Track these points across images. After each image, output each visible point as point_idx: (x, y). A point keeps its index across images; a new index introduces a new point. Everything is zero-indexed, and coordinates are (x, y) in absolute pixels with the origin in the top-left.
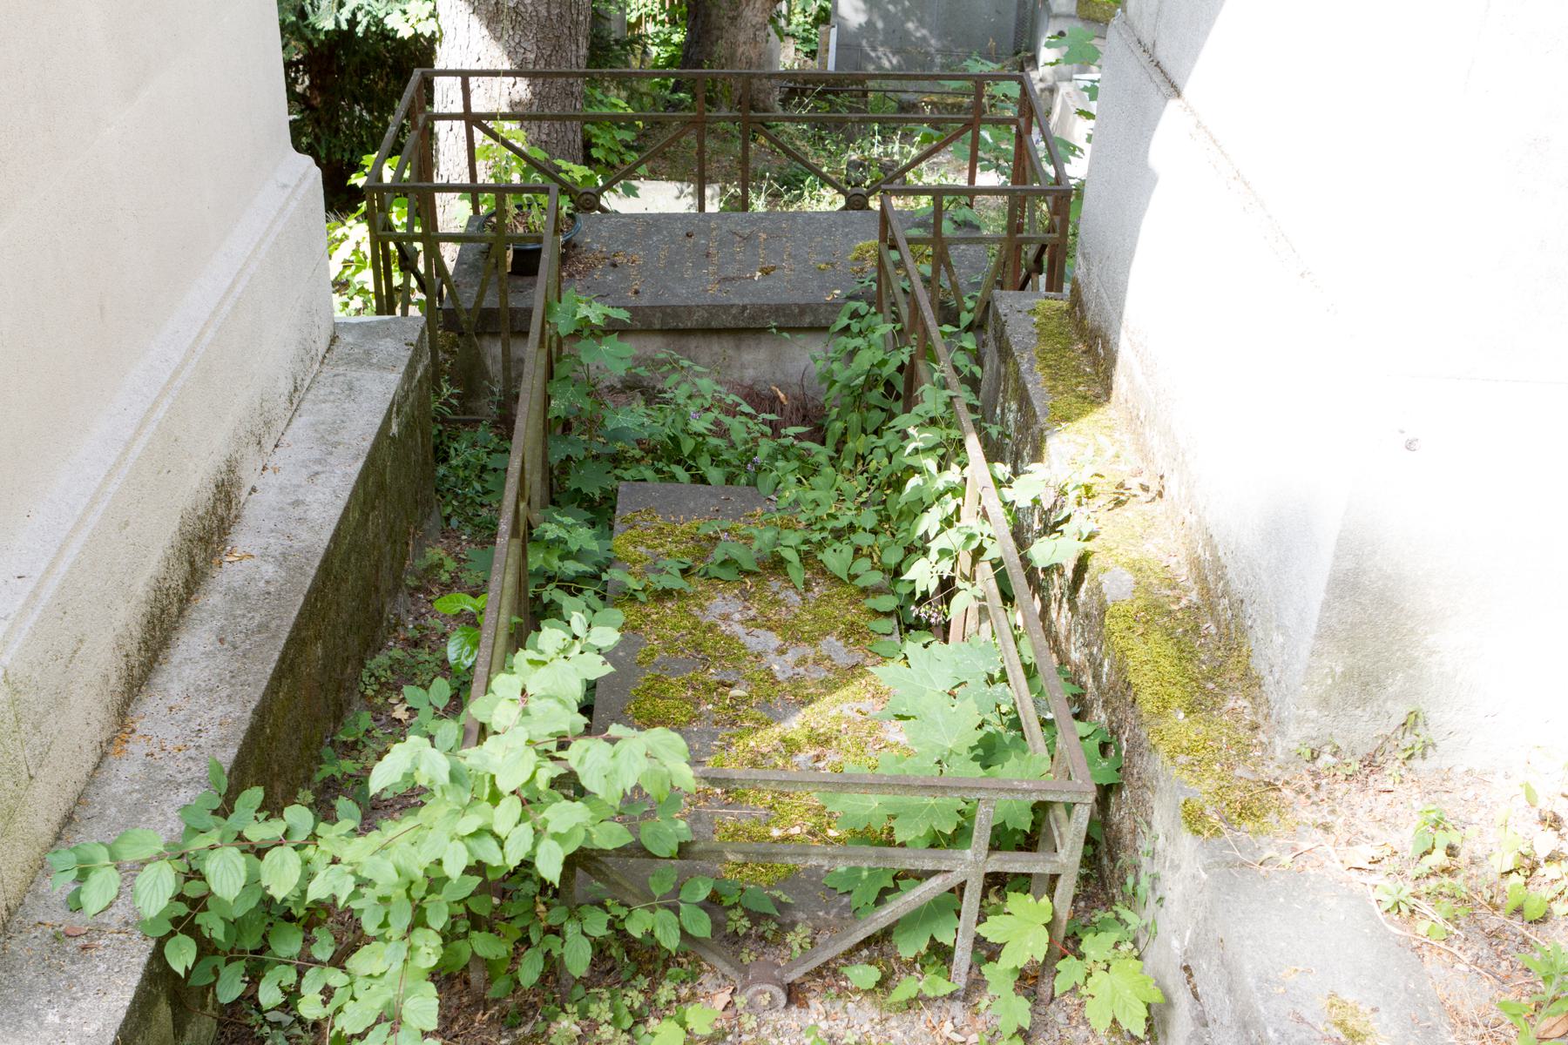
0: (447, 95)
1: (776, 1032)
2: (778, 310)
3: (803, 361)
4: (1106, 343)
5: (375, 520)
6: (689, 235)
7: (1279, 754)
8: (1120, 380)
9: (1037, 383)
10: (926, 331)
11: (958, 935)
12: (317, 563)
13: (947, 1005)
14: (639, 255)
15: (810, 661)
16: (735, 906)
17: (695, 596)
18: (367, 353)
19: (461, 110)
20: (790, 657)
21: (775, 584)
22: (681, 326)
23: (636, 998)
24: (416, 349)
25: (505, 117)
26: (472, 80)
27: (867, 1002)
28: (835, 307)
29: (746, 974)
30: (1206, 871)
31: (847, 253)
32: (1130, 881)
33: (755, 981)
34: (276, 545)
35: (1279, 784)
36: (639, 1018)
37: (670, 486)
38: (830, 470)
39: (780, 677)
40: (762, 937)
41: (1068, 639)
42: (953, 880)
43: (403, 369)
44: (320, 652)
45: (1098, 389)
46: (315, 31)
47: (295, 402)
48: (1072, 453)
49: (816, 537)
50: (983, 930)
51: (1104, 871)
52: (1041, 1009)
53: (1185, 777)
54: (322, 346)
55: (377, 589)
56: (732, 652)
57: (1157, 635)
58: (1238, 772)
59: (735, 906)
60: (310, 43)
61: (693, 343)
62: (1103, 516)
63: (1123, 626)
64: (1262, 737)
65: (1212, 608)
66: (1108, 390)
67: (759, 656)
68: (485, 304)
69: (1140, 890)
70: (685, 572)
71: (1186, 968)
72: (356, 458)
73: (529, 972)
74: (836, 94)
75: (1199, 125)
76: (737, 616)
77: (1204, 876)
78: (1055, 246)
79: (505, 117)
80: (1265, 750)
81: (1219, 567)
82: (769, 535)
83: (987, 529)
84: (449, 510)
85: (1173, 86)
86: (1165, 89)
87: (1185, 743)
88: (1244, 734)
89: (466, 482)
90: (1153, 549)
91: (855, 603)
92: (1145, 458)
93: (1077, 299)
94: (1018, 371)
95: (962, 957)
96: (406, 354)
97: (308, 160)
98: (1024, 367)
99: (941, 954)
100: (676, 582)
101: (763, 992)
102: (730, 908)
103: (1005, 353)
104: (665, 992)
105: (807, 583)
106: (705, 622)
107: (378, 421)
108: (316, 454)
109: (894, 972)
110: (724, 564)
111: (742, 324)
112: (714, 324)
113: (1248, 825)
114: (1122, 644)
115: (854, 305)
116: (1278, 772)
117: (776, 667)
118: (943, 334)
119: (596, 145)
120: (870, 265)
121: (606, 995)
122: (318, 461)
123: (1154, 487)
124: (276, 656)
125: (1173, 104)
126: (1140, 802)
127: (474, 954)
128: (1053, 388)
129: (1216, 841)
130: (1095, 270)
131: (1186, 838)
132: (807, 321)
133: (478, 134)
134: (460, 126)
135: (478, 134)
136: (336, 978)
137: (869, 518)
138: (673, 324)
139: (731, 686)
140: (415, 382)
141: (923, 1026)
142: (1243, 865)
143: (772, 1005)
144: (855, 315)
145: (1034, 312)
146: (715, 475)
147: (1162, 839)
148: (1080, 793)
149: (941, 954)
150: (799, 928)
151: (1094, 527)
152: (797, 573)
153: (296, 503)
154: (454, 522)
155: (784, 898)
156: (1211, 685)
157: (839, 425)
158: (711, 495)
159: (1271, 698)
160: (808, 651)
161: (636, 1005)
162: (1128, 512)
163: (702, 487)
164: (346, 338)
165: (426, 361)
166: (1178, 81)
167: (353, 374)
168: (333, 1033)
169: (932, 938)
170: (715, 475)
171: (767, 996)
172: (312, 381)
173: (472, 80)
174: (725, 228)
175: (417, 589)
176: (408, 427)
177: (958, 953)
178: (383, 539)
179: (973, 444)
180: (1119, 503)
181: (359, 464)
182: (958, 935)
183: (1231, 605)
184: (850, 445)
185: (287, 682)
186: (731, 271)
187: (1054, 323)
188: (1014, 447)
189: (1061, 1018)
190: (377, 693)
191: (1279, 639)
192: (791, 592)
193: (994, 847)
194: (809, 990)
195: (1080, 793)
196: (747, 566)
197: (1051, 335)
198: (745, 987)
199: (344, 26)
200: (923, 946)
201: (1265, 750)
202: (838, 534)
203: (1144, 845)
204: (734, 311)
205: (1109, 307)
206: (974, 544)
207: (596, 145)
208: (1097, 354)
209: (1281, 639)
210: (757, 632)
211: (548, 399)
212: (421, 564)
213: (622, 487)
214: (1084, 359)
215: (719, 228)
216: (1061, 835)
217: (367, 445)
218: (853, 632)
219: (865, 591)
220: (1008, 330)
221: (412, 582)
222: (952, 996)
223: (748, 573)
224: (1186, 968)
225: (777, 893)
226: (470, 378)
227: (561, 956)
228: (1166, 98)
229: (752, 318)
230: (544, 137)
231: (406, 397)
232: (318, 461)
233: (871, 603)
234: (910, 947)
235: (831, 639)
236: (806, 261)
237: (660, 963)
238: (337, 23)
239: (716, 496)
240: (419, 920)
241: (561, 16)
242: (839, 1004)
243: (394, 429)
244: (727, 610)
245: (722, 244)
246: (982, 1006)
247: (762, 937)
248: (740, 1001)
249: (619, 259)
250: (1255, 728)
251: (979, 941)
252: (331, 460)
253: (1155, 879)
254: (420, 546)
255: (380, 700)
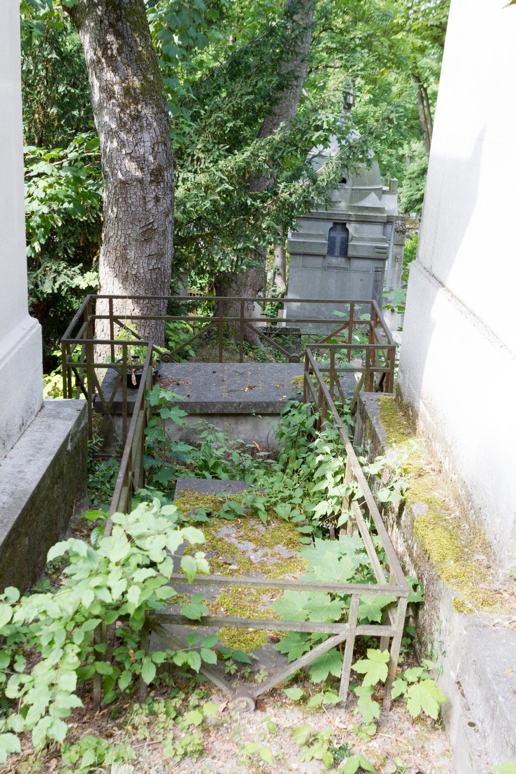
0: (102, 307)
1: (249, 722)
2: (256, 405)
3: (270, 427)
4: (413, 408)
5: (57, 491)
6: (214, 372)
7: (501, 577)
8: (420, 424)
9: (380, 428)
10: (327, 404)
11: (342, 671)
12: (28, 496)
13: (337, 711)
14: (191, 381)
15: (269, 555)
16: (229, 659)
17: (213, 526)
18: (58, 413)
19: (108, 314)
20: (260, 553)
21: (252, 522)
22: (209, 412)
23: (177, 702)
24: (81, 413)
25: (128, 317)
26: (115, 301)
27: (296, 709)
28: (283, 404)
29: (235, 692)
30: (466, 630)
31: (289, 381)
32: (429, 647)
33: (239, 695)
34: (9, 488)
35: (501, 591)
36: (179, 714)
37: (202, 480)
38: (280, 473)
39: (254, 561)
40: (243, 677)
41: (396, 543)
42: (338, 640)
43: (75, 420)
44: (27, 542)
45: (410, 430)
46: (42, 293)
47: (23, 430)
48: (396, 455)
49: (273, 500)
50: (355, 667)
51: (414, 647)
52: (385, 713)
53: (455, 588)
54: (37, 408)
55: (56, 524)
56: (231, 550)
57: (440, 529)
58: (481, 585)
59: (229, 659)
60: (38, 299)
61: (215, 420)
62: (412, 481)
63: (422, 525)
64: (492, 571)
65: (466, 516)
66: (415, 430)
67: (244, 552)
68: (115, 400)
69: (434, 652)
70: (209, 515)
71: (458, 683)
72: (50, 455)
73: (124, 683)
74: (286, 335)
75: (452, 296)
76: (234, 535)
77: (465, 632)
78: (389, 373)
79: (128, 317)
80: (494, 577)
81: (469, 497)
82: (250, 497)
83: (355, 484)
84: (93, 496)
85: (441, 283)
86: (437, 284)
87: (454, 574)
88: (484, 570)
89: (103, 483)
90: (437, 494)
91: (292, 530)
92: (433, 456)
93: (399, 394)
94: (371, 425)
95: (344, 685)
96: (77, 414)
97: (36, 321)
98: (374, 422)
99: (334, 682)
100: (205, 519)
101: (243, 701)
102: (226, 660)
103: (365, 417)
104: (193, 700)
105: (268, 522)
106: (218, 537)
107: (62, 440)
108: (31, 452)
109: (310, 695)
110: (227, 512)
111: (239, 412)
112: (225, 411)
113: (487, 608)
114: (422, 533)
115: (292, 402)
116: (501, 586)
117: (252, 557)
118: (335, 405)
119: (170, 340)
120: (301, 385)
121: (163, 701)
122: (32, 455)
123: (437, 468)
124: (6, 534)
125: (441, 295)
126: (434, 608)
127: (96, 672)
128: (387, 430)
129: (470, 615)
130: (407, 376)
131: (457, 616)
132: (270, 410)
133: (116, 326)
134: (107, 321)
135: (116, 326)
136: (25, 679)
137: (299, 493)
138: (205, 411)
139: (230, 564)
140: (80, 429)
141: (325, 721)
142: (484, 626)
143: (247, 709)
144: (293, 406)
145: (379, 400)
146: (224, 476)
147: (444, 621)
148: (402, 591)
149: (334, 682)
150: (261, 672)
151: (408, 486)
152: (264, 516)
153: (20, 472)
154: (96, 502)
155: (254, 657)
156: (466, 550)
157: (285, 456)
158: (222, 484)
159: (496, 551)
160: (269, 551)
161: (178, 705)
162: (425, 480)
163: (218, 481)
164: (48, 407)
165: (86, 420)
166: (442, 280)
167: (50, 421)
168: (23, 705)
169: (330, 674)
170: (224, 476)
171: (245, 703)
172: (31, 423)
173: (115, 301)
174: (231, 369)
175: (76, 530)
176: (76, 448)
177: (342, 681)
178: (60, 500)
179: (349, 448)
180: (420, 476)
181: (52, 458)
182: (342, 671)
183: (475, 512)
184: (290, 465)
185: (10, 550)
186: (233, 387)
187: (389, 404)
188: (370, 445)
189: (395, 717)
190: (54, 573)
191: (498, 520)
192: (261, 526)
193: (359, 623)
194: (266, 703)
195: (402, 591)
196: (239, 513)
197: (387, 409)
198: (234, 698)
199: (56, 291)
200: (325, 677)
201: (494, 577)
202: (284, 500)
203: (435, 627)
204: (235, 405)
205: (414, 391)
206: (350, 492)
207: (170, 340)
208: (409, 415)
209: (499, 521)
210: (243, 542)
211: (144, 436)
212: (79, 517)
213: (179, 480)
214: (403, 418)
215: (229, 369)
216: (393, 618)
217: (56, 450)
218: (291, 543)
219: (297, 525)
220: (366, 407)
221: (73, 526)
222: (338, 705)
223: (240, 517)
224: (458, 683)
225: (251, 654)
226: (108, 435)
227: (141, 673)
228: (437, 287)
229: (244, 408)
230: (147, 335)
231: (76, 434)
232: (32, 455)
233: (300, 529)
234: (318, 677)
235: (280, 546)
236: (270, 384)
237: (191, 688)
238: (53, 290)
239: (225, 484)
240: (69, 638)
241: (157, 279)
242: (282, 710)
243: (69, 448)
244: (229, 532)
245: (230, 376)
246: (355, 712)
247: (243, 677)
248: (230, 705)
249: (180, 382)
250: (489, 567)
251: (352, 672)
252: (38, 455)
253: (442, 643)
254: (78, 512)
255: (55, 576)
